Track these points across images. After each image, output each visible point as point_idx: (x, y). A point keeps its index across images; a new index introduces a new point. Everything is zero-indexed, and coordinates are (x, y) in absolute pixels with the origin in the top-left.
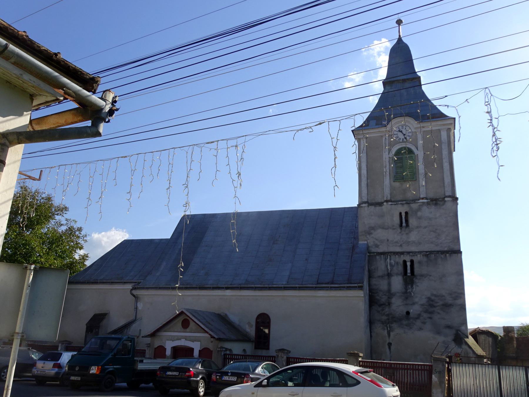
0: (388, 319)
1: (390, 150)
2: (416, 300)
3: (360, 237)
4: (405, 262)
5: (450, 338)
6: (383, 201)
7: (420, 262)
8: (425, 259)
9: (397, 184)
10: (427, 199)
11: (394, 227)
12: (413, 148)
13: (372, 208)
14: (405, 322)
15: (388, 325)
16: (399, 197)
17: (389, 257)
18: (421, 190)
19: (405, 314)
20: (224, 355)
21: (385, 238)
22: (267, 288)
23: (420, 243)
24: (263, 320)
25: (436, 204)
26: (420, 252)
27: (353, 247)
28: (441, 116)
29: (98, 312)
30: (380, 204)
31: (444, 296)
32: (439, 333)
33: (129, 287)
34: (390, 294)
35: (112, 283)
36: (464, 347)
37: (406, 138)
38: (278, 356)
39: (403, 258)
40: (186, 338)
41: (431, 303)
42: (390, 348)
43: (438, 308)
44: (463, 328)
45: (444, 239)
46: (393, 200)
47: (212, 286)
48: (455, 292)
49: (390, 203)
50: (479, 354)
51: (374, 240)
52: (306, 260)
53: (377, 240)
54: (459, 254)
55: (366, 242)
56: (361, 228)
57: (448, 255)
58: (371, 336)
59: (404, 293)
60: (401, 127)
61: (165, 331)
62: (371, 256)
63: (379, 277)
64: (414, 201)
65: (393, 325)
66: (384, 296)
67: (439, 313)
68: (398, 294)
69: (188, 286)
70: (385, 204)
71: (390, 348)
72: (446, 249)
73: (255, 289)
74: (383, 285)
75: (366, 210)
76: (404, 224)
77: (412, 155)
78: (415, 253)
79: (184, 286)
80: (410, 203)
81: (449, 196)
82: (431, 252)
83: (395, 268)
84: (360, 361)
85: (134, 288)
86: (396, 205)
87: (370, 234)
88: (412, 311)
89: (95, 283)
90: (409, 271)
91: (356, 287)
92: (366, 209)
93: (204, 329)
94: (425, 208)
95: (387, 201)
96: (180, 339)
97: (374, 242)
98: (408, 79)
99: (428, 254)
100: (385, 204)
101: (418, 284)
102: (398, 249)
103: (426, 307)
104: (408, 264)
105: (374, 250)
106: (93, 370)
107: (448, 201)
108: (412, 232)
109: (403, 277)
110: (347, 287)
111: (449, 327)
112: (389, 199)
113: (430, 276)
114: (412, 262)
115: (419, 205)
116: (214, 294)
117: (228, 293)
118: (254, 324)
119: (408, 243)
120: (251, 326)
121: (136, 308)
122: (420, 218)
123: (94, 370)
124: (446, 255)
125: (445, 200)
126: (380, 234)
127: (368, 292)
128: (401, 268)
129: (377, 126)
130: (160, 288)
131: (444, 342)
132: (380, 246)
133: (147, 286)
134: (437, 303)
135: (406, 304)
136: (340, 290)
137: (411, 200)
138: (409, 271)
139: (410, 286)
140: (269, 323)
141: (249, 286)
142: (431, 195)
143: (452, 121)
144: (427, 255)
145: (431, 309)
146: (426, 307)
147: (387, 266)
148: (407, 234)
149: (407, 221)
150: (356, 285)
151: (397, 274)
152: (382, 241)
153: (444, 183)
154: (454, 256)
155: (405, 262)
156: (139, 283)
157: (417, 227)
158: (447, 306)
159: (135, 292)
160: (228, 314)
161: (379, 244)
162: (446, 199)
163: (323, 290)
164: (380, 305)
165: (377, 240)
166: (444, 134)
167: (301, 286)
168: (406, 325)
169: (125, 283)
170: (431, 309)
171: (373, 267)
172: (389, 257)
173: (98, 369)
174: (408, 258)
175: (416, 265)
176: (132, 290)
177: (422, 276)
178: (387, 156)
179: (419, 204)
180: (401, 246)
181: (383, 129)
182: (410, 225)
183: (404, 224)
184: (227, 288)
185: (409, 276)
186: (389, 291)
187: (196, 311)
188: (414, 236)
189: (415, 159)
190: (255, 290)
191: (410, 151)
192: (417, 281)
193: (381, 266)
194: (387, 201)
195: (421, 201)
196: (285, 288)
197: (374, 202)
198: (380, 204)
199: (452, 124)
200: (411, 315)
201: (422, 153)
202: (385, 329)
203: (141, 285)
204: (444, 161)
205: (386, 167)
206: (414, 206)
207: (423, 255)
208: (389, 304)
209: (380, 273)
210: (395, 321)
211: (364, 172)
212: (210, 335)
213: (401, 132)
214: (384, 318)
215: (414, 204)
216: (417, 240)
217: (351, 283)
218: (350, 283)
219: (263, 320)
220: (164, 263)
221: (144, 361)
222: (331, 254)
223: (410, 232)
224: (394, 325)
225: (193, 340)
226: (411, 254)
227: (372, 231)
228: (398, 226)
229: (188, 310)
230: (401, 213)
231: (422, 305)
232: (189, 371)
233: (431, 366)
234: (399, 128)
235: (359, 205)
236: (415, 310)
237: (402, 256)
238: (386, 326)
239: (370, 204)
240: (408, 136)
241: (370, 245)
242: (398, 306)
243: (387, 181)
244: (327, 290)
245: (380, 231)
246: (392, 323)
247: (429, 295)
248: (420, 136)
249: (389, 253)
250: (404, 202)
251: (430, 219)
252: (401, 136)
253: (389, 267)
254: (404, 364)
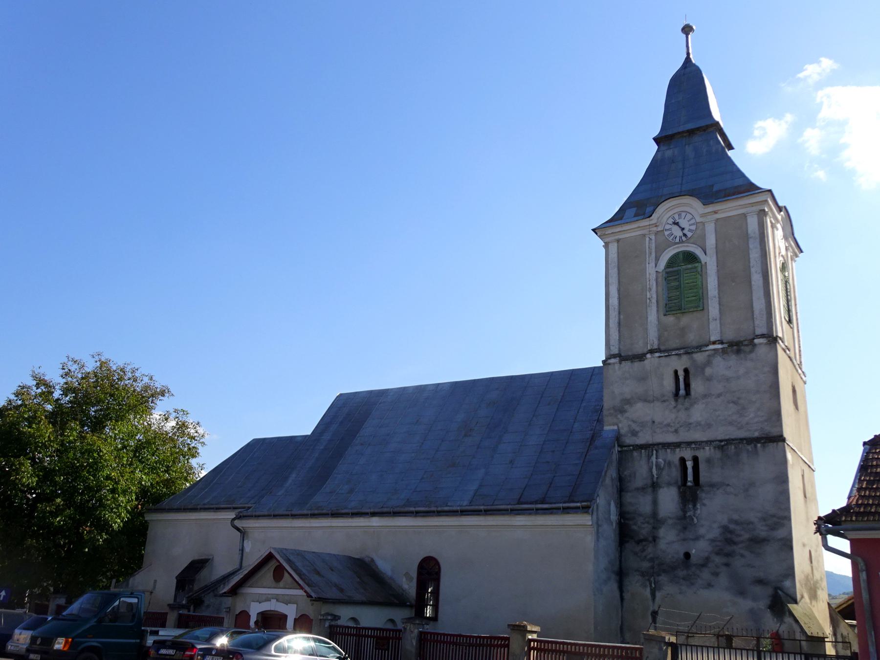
0: (653, 567)
1: (657, 259)
2: (702, 531)
3: (605, 419)
4: (683, 461)
5: (762, 604)
6: (645, 351)
7: (709, 461)
8: (718, 454)
9: (671, 319)
10: (722, 343)
11: (666, 398)
12: (698, 252)
13: (627, 365)
14: (681, 573)
15: (652, 579)
16: (674, 343)
17: (655, 452)
19: (682, 556)
20: (331, 626)
21: (645, 415)
22: (434, 512)
23: (709, 426)
24: (429, 571)
25: (738, 352)
26: (709, 442)
27: (593, 436)
28: (750, 188)
29: (196, 558)
30: (641, 357)
31: (752, 523)
32: (742, 593)
33: (232, 515)
34: (656, 521)
35: (218, 509)
36: (788, 620)
37: (685, 235)
38: (405, 629)
40: (278, 598)
41: (729, 536)
43: (740, 546)
44: (787, 583)
45: (752, 415)
46: (662, 348)
47: (350, 511)
48: (773, 516)
49: (657, 355)
50: (809, 634)
51: (630, 423)
52: (511, 462)
53: (634, 422)
54: (780, 444)
55: (615, 428)
56: (608, 403)
57: (759, 445)
58: (622, 599)
60: (676, 217)
61: (251, 587)
62: (626, 451)
63: (637, 489)
64: (699, 348)
65: (660, 578)
66: (646, 525)
67: (742, 556)
68: (670, 522)
69: (316, 512)
70: (649, 356)
72: (756, 434)
73: (417, 514)
74: (643, 504)
75: (619, 369)
76: (682, 392)
77: (696, 265)
78: (699, 444)
79: (309, 512)
80: (692, 353)
81: (762, 336)
82: (729, 442)
83: (664, 473)
84: (530, 640)
85: (239, 517)
86: (667, 359)
87: (622, 411)
88: (694, 551)
89: (194, 509)
90: (690, 478)
91: (578, 508)
92: (617, 366)
93: (299, 585)
94: (718, 360)
95: (652, 351)
96: (268, 600)
97: (629, 426)
98: (698, 129)
99: (722, 445)
100: (649, 356)
101: (705, 502)
102: (671, 438)
103: (718, 543)
104: (689, 464)
105: (629, 440)
106: (59, 643)
107: (760, 344)
109: (679, 488)
110: (564, 508)
111: (760, 582)
112: (656, 347)
113: (728, 485)
114: (695, 460)
115: (709, 356)
116: (354, 524)
117: (375, 522)
118: (414, 574)
119: (688, 426)
120: (410, 579)
121: (242, 550)
122: (709, 379)
123: (60, 644)
124: (756, 446)
125: (756, 343)
126: (639, 411)
127: (614, 517)
128: (676, 473)
129: (636, 218)
130: (275, 516)
131: (752, 611)
132: (640, 434)
133: (257, 514)
134: (740, 536)
135: (684, 540)
136: (551, 513)
137: (694, 348)
138: (690, 478)
139: (690, 506)
140: (438, 573)
141: (407, 509)
142: (730, 335)
144: (723, 446)
145: (728, 549)
147: (651, 469)
148: (687, 409)
149: (687, 385)
150: (579, 504)
151: (669, 484)
152: (643, 425)
153: (753, 312)
154: (771, 446)
155: (683, 461)
156: (249, 508)
158: (757, 542)
159: (237, 523)
160: (375, 558)
161: (637, 429)
162: (756, 341)
163: (524, 514)
164: (639, 542)
165: (634, 422)
166: (752, 223)
167: (489, 507)
168: (684, 579)
169: (217, 509)
170: (728, 549)
172: (655, 452)
173: (66, 642)
174: (688, 454)
175: (702, 467)
176: (234, 519)
177: (712, 485)
178: (653, 269)
179: (707, 353)
180: (676, 431)
181: (646, 222)
182: (693, 393)
183: (682, 392)
184: (374, 514)
185: (689, 487)
186: (655, 514)
187: (300, 554)
188: (698, 413)
189: (701, 272)
190: (416, 516)
191: (690, 258)
192: (703, 495)
193: (641, 469)
194: (652, 351)
195: (712, 347)
196: (463, 513)
197: (630, 354)
198: (641, 357)
200: (694, 559)
201: (714, 258)
202: (645, 586)
203: (249, 512)
204: (753, 270)
205: (650, 289)
206: (700, 357)
207: (715, 448)
208: (655, 539)
209: (639, 482)
210: (664, 571)
211: (614, 301)
212: (305, 592)
213: (677, 224)
214: (646, 565)
215: (699, 354)
216: (707, 418)
217: (573, 502)
218: (576, 500)
219: (429, 571)
220: (294, 475)
221: (160, 633)
222: (553, 451)
223: (692, 405)
224: (663, 578)
225: (287, 601)
227: (626, 407)
228: (671, 395)
229: (281, 551)
230: (676, 372)
231: (713, 540)
232: (193, 647)
233: (641, 650)
234: (673, 218)
235: (604, 362)
236: (699, 549)
237: (678, 450)
238: (649, 580)
239: (622, 358)
240: (690, 230)
241: (623, 432)
242: (669, 544)
243: (653, 315)
244: (530, 514)
245: (639, 405)
246: (659, 575)
247: (725, 521)
248: (710, 229)
249: (653, 445)
250: (682, 351)
251: (728, 380)
252: (677, 232)
254: (576, 645)
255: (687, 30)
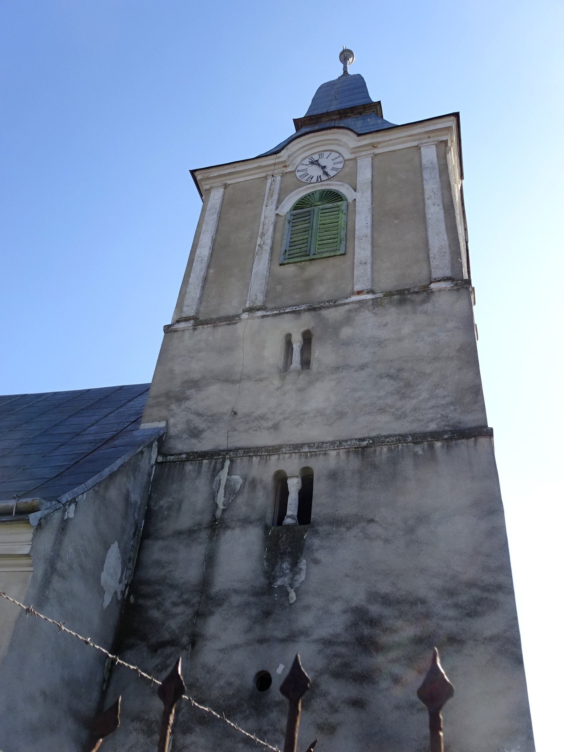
2: (305, 620)
4: (281, 480)
8: (355, 463)
12: (344, 190)
18: (356, 273)
26: (337, 444)
31: (423, 602)
34: (205, 599)
37: (326, 173)
39: (275, 464)
41: (366, 631)
43: (392, 655)
45: (425, 395)
49: (260, 313)
51: (192, 417)
54: (483, 440)
55: (163, 424)
57: (438, 444)
59: (259, 593)
63: (179, 533)
70: (245, 316)
72: (432, 427)
74: (183, 564)
77: (339, 203)
78: (318, 448)
80: (320, 308)
82: (377, 441)
83: (240, 500)
86: (277, 319)
87: (181, 398)
90: (292, 509)
94: (366, 316)
99: (363, 449)
103: (342, 650)
104: (294, 485)
105: (182, 446)
107: (440, 290)
108: (318, 385)
113: (371, 521)
114: (307, 480)
115: (350, 311)
124: (431, 447)
128: (263, 500)
134: (392, 630)
135: (262, 641)
138: (292, 509)
139: (286, 565)
142: (388, 282)
143: (451, 123)
146: (342, 650)
148: (301, 390)
152: (214, 419)
154: (464, 446)
155: (281, 480)
157: (337, 369)
161: (202, 426)
162: (433, 286)
165: (199, 414)
171: (164, 503)
172: (228, 463)
174: (292, 466)
177: (337, 522)
179: (347, 307)
182: (314, 365)
186: (205, 583)
193: (193, 496)
194: (251, 310)
199: (449, 128)
205: (263, 234)
206: (332, 314)
207: (348, 452)
208: (195, 640)
209: (185, 521)
215: (332, 310)
223: (311, 383)
226: (306, 449)
231: (328, 642)
241: (173, 431)
242: (227, 650)
243: (261, 265)
249: (228, 451)
251: (380, 343)
253: (221, 499)
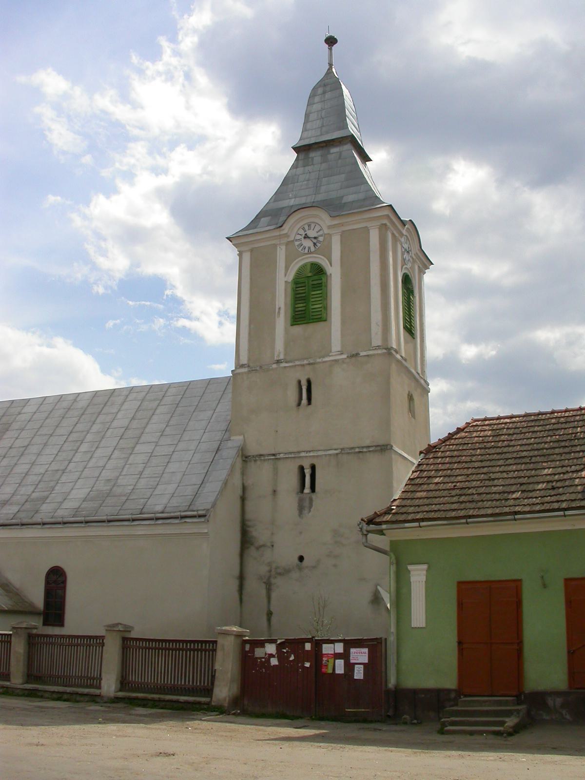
9: (298, 330)
24: (56, 579)
42: (269, 620)
60: (306, 227)
71: (269, 620)
255: (331, 41)
